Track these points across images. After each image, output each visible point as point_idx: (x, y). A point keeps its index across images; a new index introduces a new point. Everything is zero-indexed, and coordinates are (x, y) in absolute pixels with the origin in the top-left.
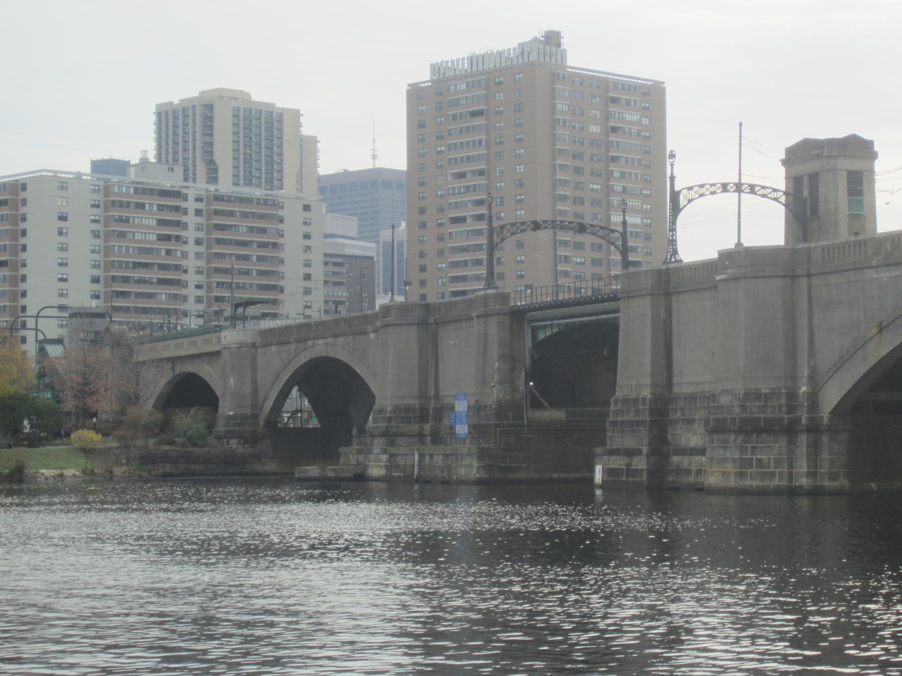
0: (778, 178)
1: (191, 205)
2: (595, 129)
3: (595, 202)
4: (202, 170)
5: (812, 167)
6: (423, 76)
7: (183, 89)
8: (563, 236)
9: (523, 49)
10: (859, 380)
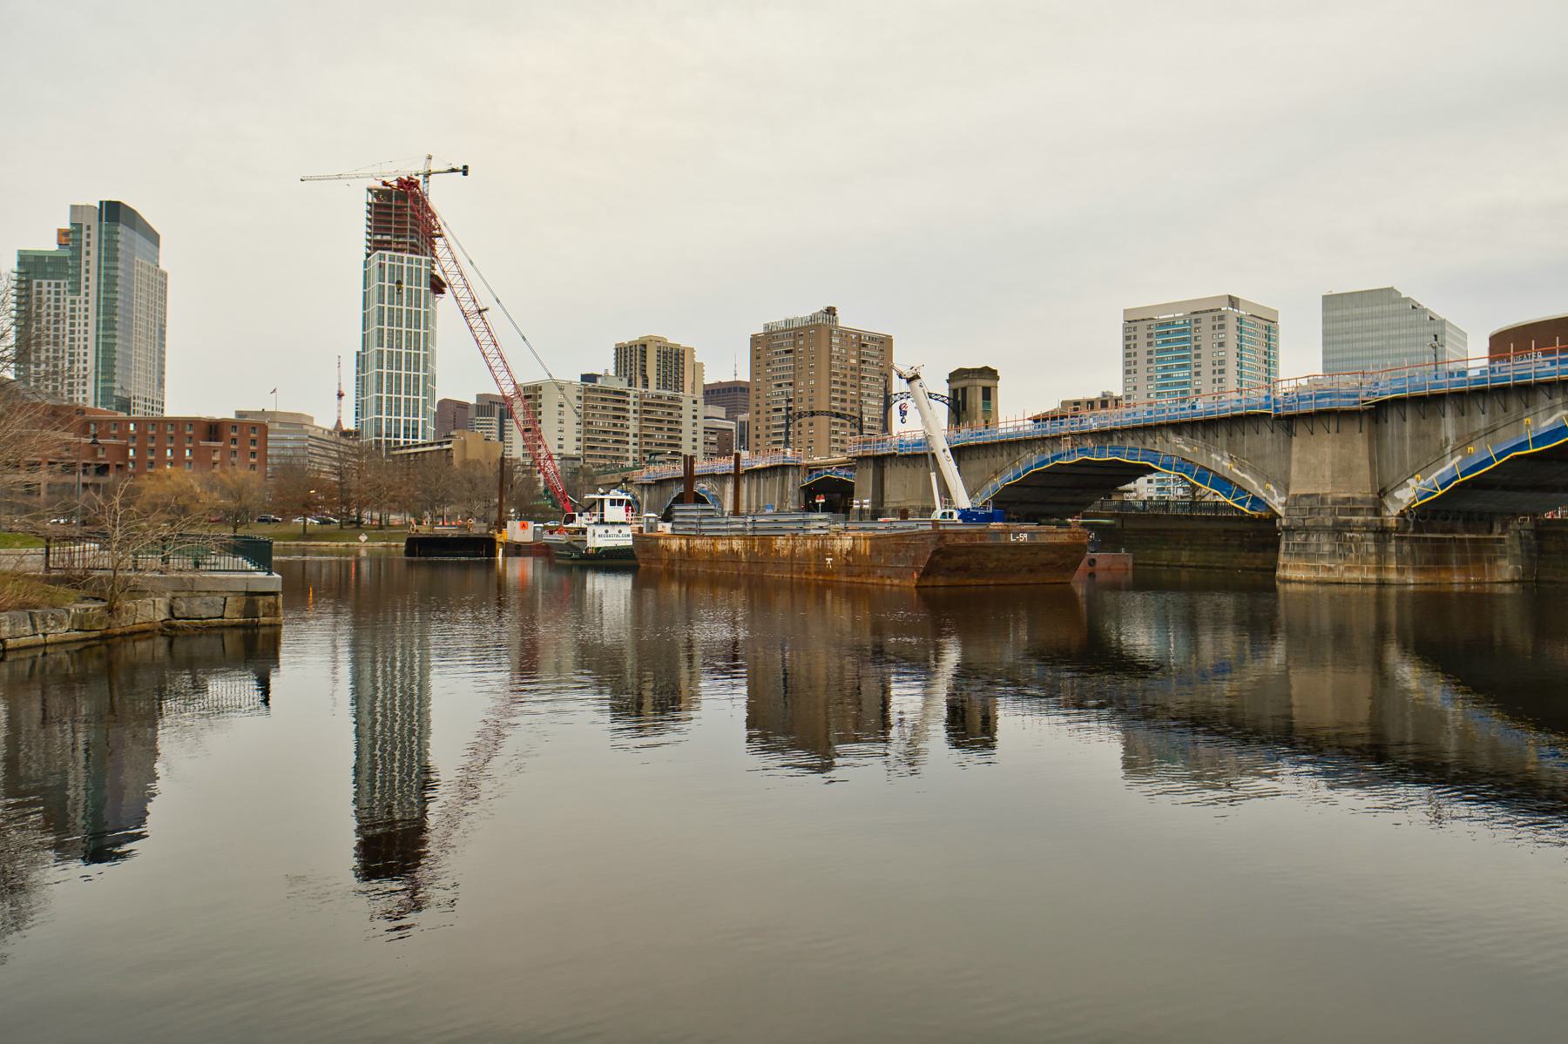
0: (944, 390)
1: (631, 399)
2: (853, 361)
3: (853, 401)
4: (640, 381)
5: (959, 384)
6: (760, 330)
7: (629, 337)
8: (834, 420)
9: (814, 317)
10: (164, 298)
